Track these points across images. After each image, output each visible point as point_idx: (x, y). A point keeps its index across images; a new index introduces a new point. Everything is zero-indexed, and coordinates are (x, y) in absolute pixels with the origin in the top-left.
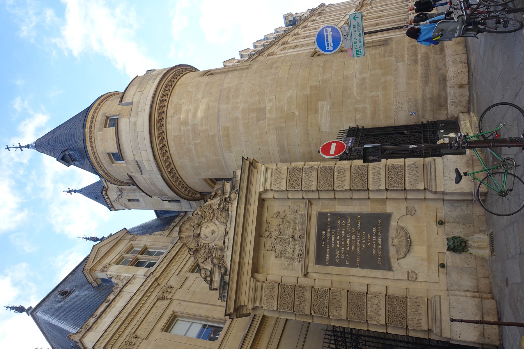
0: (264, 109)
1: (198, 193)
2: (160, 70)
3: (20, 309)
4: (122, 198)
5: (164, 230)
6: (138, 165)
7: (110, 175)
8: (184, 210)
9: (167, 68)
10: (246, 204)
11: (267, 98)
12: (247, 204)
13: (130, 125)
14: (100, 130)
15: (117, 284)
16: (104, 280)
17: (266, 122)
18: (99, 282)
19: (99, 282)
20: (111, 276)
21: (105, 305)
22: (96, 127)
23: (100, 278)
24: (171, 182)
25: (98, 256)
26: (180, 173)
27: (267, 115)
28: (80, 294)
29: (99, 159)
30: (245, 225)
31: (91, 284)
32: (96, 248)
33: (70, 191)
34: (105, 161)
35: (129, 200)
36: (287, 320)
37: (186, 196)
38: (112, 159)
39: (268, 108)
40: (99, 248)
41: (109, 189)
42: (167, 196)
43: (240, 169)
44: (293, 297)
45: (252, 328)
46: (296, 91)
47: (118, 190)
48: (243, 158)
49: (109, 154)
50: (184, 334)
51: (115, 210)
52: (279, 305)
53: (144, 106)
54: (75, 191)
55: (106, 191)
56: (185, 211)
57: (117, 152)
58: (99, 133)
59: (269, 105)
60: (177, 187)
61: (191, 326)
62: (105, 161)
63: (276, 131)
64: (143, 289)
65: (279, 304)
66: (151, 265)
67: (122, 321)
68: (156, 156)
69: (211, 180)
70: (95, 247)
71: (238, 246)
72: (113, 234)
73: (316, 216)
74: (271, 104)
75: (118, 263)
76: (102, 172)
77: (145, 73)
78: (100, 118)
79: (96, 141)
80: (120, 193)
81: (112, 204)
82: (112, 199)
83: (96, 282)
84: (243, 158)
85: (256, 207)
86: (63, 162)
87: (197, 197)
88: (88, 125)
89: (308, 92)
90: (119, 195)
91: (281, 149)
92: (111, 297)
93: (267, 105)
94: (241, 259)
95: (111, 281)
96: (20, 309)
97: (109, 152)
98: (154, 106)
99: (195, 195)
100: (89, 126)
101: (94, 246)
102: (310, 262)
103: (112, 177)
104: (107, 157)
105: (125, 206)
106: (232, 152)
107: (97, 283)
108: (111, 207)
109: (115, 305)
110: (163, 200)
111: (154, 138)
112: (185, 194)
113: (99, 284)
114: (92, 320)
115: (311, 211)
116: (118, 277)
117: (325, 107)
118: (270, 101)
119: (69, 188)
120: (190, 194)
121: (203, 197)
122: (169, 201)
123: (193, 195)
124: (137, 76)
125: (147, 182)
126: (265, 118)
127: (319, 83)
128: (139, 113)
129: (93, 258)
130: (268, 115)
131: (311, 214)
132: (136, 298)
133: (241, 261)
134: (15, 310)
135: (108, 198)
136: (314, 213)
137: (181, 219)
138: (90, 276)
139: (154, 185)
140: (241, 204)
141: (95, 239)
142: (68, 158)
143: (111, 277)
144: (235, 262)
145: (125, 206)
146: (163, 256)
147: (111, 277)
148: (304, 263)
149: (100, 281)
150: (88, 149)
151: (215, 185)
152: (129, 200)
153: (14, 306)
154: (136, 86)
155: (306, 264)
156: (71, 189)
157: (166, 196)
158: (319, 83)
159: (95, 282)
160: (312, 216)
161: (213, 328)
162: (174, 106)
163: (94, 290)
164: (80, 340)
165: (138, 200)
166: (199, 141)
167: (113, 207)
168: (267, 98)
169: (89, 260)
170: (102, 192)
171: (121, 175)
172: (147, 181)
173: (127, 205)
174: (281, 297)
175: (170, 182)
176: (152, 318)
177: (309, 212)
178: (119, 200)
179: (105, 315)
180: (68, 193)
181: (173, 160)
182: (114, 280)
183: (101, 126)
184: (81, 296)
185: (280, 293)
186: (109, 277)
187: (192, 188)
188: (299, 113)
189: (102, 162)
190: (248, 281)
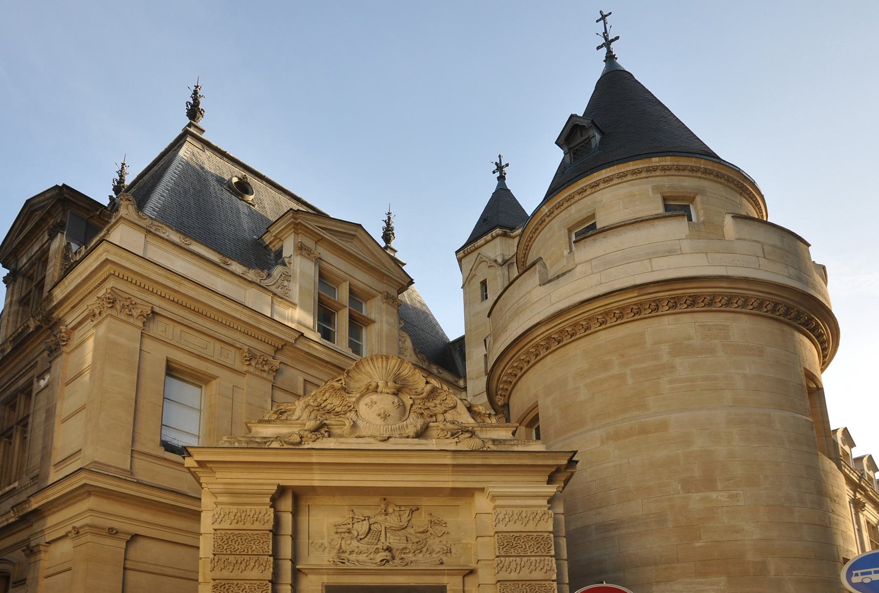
0: (713, 489)
1: (506, 400)
2: (826, 291)
3: (194, 111)
4: (489, 267)
5: (416, 354)
6: (563, 274)
7: (540, 228)
8: (469, 385)
9: (831, 307)
10: (454, 466)
11: (741, 492)
12: (455, 469)
13: (669, 242)
14: (656, 189)
15: (269, 275)
16: (279, 253)
17: (679, 493)
18: (274, 246)
19: (274, 246)
20: (288, 264)
21: (215, 257)
22: (665, 179)
23: (282, 246)
24: (526, 345)
25: (335, 235)
26: (549, 357)
27: (695, 494)
28: (242, 216)
29: (579, 200)
30: (401, 468)
31: (267, 232)
32: (356, 231)
33: (500, 168)
34: (576, 212)
35: (484, 284)
36: (198, 548)
37: (496, 379)
38: (580, 226)
39: (714, 495)
40: (354, 236)
41: (510, 241)
42: (494, 342)
43: (546, 448)
44: (244, 553)
45: (149, 491)
46: (755, 538)
47: (507, 258)
48: (575, 452)
49: (593, 216)
50: (166, 397)
51: (460, 261)
52: (223, 532)
53: (723, 264)
54: (502, 178)
55: (505, 235)
56: (466, 387)
57: (597, 228)
58: (649, 187)
59: (722, 496)
60: (516, 357)
61: (197, 409)
62: (573, 211)
63: (655, 514)
64: (259, 321)
65: (227, 531)
66: (327, 334)
67: (176, 288)
68: (590, 305)
69: (536, 418)
70: (359, 229)
71: (350, 459)
72: (404, 268)
73: (439, 583)
74: (723, 499)
75: (323, 277)
76: (546, 211)
77: (817, 262)
78: (687, 183)
79: (625, 184)
80: (500, 260)
81: (472, 252)
82: (483, 250)
83: (273, 241)
84: (575, 452)
85: (450, 485)
86: (568, 129)
87: (497, 399)
88: (670, 161)
89: (750, 557)
90: (496, 261)
91: (611, 525)
92: (236, 267)
93: (722, 493)
94: (319, 467)
95: (276, 264)
96: (194, 111)
97: (597, 216)
98: (724, 284)
99: (501, 395)
100: (668, 163)
101: (360, 225)
102: (330, 577)
103: (536, 234)
104: (584, 214)
105: (470, 276)
106: (603, 443)
107: (270, 243)
108: (463, 254)
109: (218, 276)
110: (485, 341)
111: (636, 294)
112: (500, 375)
113: (270, 247)
114: (175, 237)
115: (449, 575)
116: (287, 277)
117: (710, 587)
118: (731, 497)
119: (507, 165)
120: (501, 386)
121: (502, 410)
122: (486, 356)
123: (499, 393)
124: (809, 245)
125: (522, 300)
126: (689, 492)
127: (772, 574)
128: (704, 255)
129: (329, 227)
130: (696, 496)
131: (444, 574)
132: (237, 310)
133: (315, 467)
134: (192, 102)
135: (487, 242)
136: (444, 580)
137: (447, 381)
138: (284, 226)
139: (516, 314)
140: (454, 458)
141: (388, 235)
142: (579, 139)
143: (285, 265)
144: (311, 455)
145: (470, 276)
146: (351, 353)
147: (285, 265)
148: (324, 568)
149: (277, 247)
150: (604, 171)
151: (527, 426)
152: (484, 284)
153: (200, 100)
154: (779, 244)
155: (325, 571)
156: (505, 170)
157: (492, 342)
158: (772, 574)
159: (273, 238)
160: (441, 577)
161: (42, 387)
162: (725, 324)
163: (256, 240)
164: (121, 217)
165: (487, 298)
166: (630, 381)
167: (466, 255)
168: (741, 492)
169: (321, 220)
170: (501, 227)
171: (541, 251)
172: (524, 298)
173: (474, 280)
174: (238, 535)
175: (525, 343)
176: (195, 342)
177: (446, 572)
178: (484, 263)
179: (188, 259)
180: (496, 164)
181: (582, 341)
182: (278, 271)
183: (668, 188)
184: (238, 218)
185: (250, 532)
186: (286, 260)
187: (517, 386)
188: (700, 547)
189: (573, 206)
190: (270, 481)
